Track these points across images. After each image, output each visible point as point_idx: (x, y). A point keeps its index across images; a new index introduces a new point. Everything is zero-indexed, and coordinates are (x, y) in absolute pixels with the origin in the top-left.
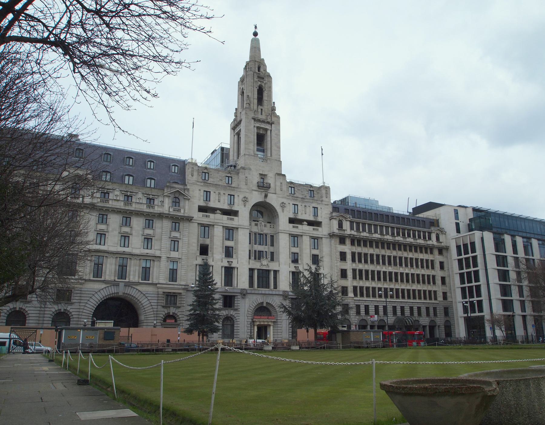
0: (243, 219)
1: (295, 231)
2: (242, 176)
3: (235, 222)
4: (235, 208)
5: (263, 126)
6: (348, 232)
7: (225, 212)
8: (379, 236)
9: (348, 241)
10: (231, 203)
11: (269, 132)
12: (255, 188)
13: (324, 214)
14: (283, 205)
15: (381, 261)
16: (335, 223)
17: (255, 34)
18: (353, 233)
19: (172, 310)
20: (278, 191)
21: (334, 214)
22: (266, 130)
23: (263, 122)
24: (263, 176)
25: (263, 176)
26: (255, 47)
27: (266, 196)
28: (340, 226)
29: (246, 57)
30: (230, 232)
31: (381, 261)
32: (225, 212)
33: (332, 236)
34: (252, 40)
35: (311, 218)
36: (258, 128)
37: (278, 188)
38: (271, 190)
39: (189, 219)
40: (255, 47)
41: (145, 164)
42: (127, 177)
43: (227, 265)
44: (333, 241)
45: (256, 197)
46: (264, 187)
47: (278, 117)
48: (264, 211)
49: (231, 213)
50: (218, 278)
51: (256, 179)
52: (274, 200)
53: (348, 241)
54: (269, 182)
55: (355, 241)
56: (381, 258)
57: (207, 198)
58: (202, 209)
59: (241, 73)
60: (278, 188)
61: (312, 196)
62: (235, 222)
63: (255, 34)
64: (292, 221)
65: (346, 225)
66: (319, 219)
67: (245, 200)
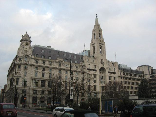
0: (98, 72)
1: (110, 75)
2: (97, 60)
3: (96, 73)
4: (96, 69)
5: (101, 45)
6: (123, 76)
7: (93, 70)
8: (130, 77)
9: (123, 78)
10: (95, 68)
11: (103, 47)
12: (100, 63)
13: (117, 70)
14: (107, 69)
15: (130, 84)
16: (120, 73)
17: (97, 17)
18: (124, 76)
19: (83, 98)
20: (106, 64)
21: (119, 70)
22: (102, 46)
23: (101, 44)
24: (102, 60)
25: (102, 60)
26: (97, 21)
27: (103, 66)
28: (121, 74)
29: (94, 24)
30: (95, 75)
31: (130, 84)
32: (93, 70)
33: (119, 77)
34: (96, 19)
35: (114, 72)
36: (100, 46)
37: (106, 63)
38: (104, 64)
39: (86, 72)
40: (97, 21)
41: (57, 53)
42: (43, 56)
43: (95, 85)
44: (119, 78)
45: (101, 66)
46: (102, 63)
47: (105, 42)
48: (102, 70)
49: (95, 70)
50: (92, 89)
51: (100, 61)
52: (105, 67)
53: (123, 78)
54: (104, 61)
55: (125, 78)
56: (128, 82)
57: (110, 70)
58: (88, 69)
59: (93, 28)
60: (106, 63)
61: (113, 65)
62: (96, 73)
63: (97, 17)
64: (109, 72)
65: (122, 74)
66: (115, 72)
67: (98, 67)
